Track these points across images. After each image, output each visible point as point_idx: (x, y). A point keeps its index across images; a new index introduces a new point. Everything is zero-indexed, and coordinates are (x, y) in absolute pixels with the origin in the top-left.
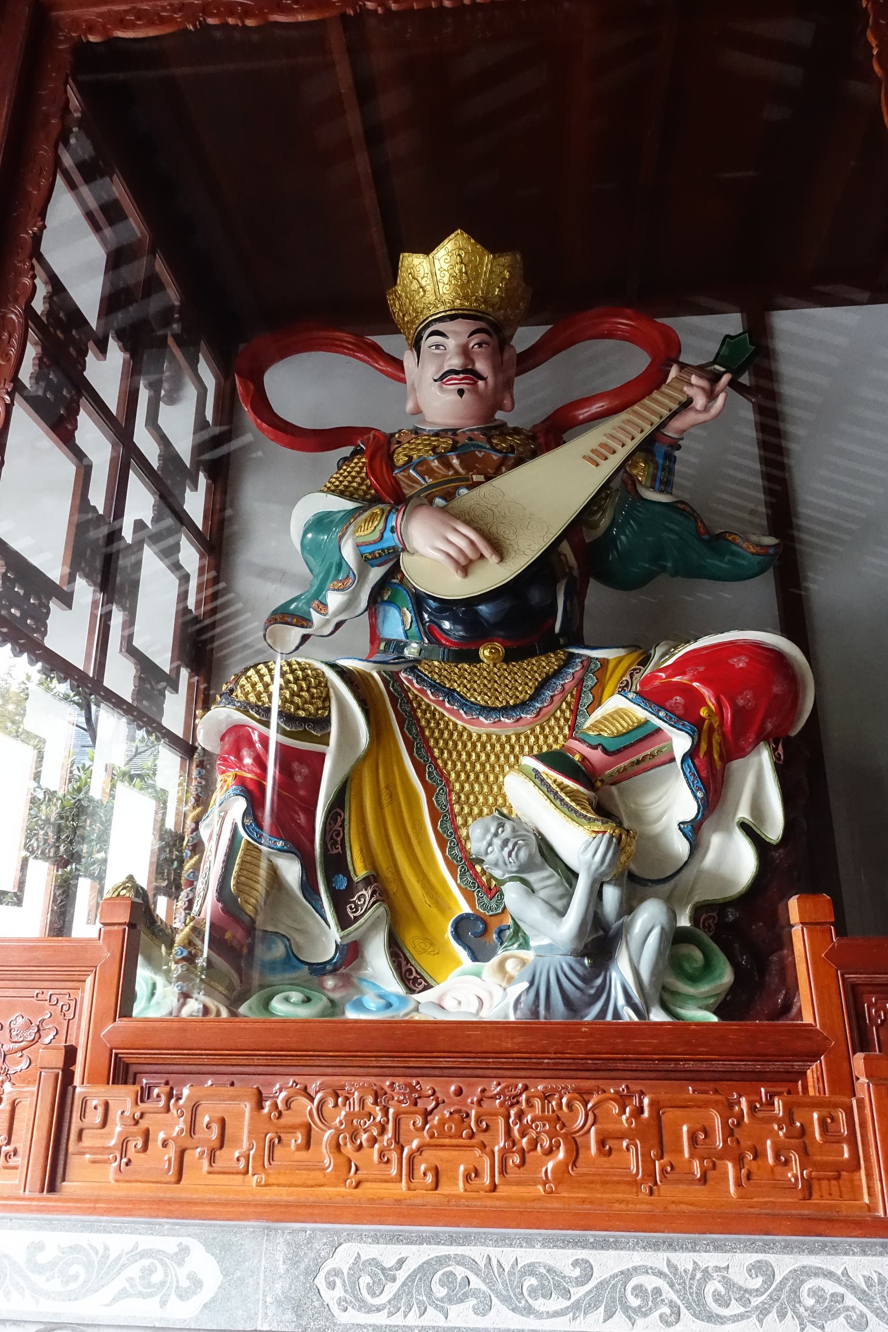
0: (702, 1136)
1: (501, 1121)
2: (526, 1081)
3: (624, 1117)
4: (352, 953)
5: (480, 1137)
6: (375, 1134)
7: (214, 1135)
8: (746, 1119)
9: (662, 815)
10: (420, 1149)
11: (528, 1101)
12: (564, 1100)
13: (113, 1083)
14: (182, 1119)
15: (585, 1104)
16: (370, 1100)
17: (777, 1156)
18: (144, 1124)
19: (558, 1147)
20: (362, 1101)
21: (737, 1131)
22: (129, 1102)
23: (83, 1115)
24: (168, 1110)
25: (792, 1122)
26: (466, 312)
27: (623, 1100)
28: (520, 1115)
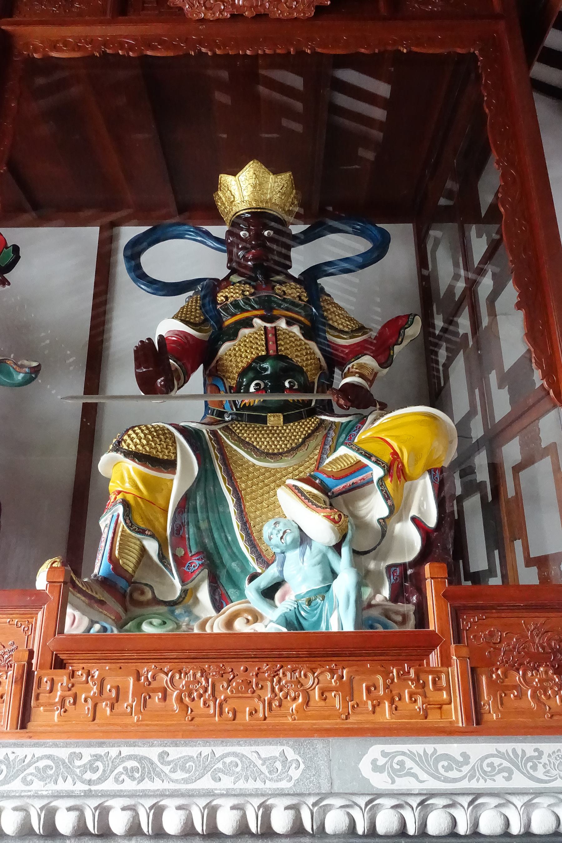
0: (373, 689)
1: (269, 684)
2: (282, 663)
3: (333, 680)
4: (188, 595)
5: (259, 692)
6: (201, 692)
7: (114, 695)
8: (396, 680)
9: (367, 514)
10: (225, 700)
11: (284, 673)
12: (302, 673)
13: (54, 669)
14: (95, 687)
15: (314, 673)
16: (199, 675)
17: (410, 698)
18: (74, 690)
19: (299, 697)
20: (194, 675)
21: (391, 686)
22: (65, 679)
23: (39, 685)
24: (87, 682)
25: (418, 680)
26: (253, 210)
27: (332, 672)
28: (279, 681)
